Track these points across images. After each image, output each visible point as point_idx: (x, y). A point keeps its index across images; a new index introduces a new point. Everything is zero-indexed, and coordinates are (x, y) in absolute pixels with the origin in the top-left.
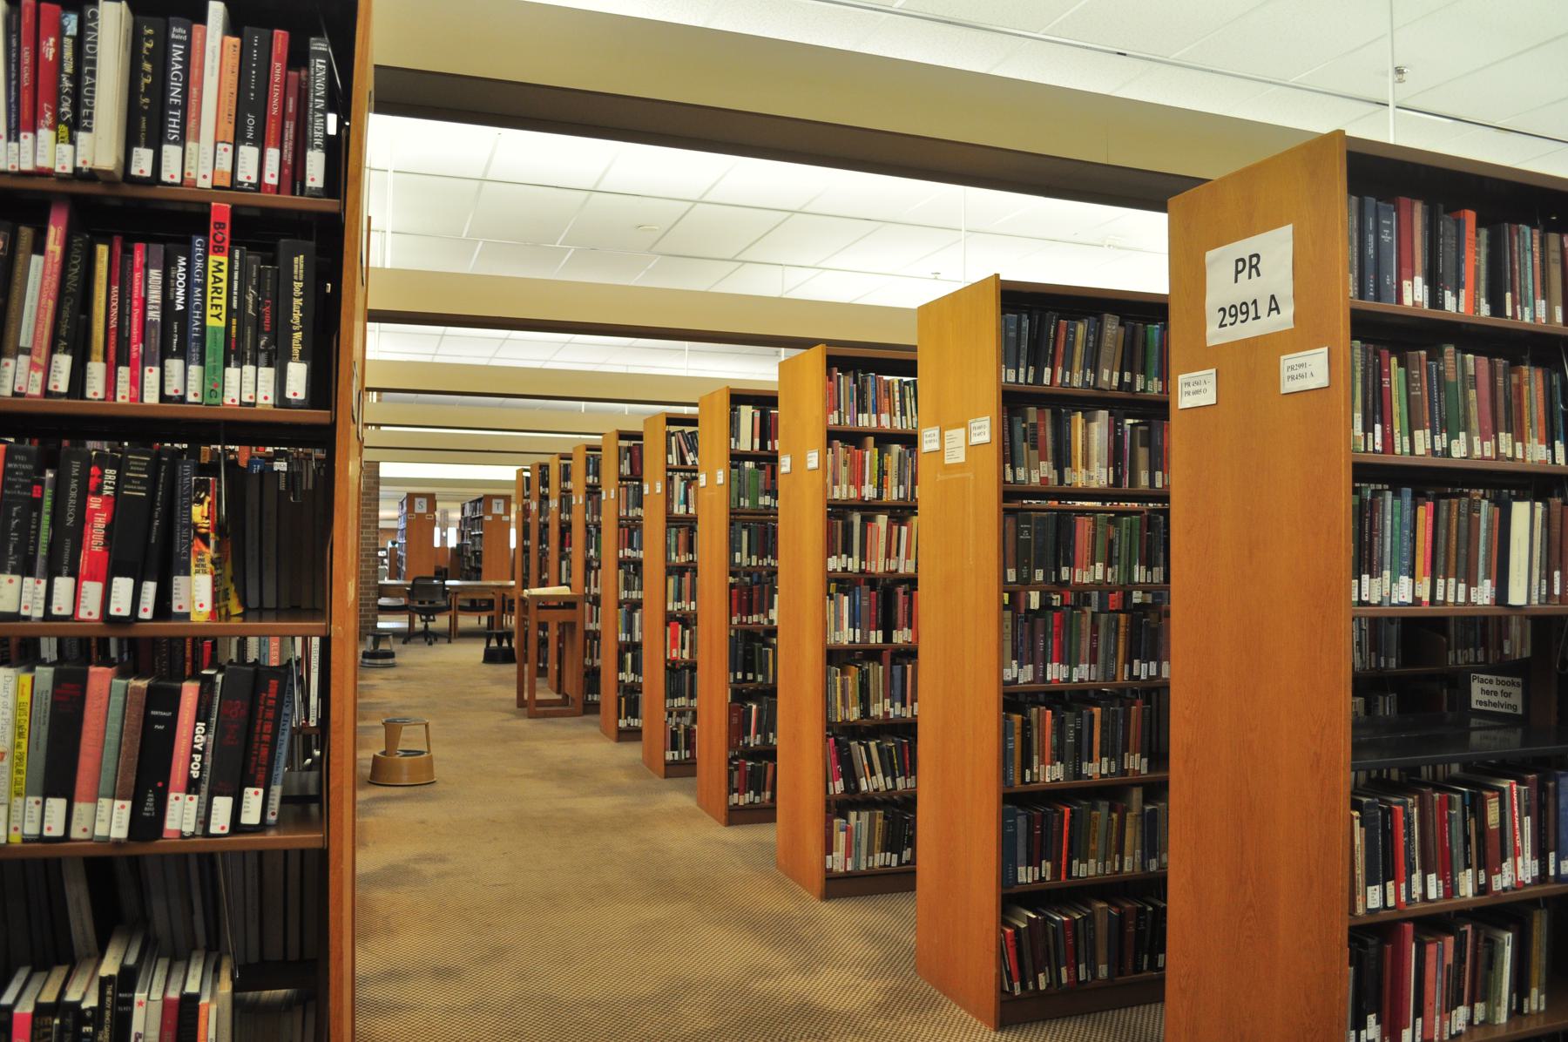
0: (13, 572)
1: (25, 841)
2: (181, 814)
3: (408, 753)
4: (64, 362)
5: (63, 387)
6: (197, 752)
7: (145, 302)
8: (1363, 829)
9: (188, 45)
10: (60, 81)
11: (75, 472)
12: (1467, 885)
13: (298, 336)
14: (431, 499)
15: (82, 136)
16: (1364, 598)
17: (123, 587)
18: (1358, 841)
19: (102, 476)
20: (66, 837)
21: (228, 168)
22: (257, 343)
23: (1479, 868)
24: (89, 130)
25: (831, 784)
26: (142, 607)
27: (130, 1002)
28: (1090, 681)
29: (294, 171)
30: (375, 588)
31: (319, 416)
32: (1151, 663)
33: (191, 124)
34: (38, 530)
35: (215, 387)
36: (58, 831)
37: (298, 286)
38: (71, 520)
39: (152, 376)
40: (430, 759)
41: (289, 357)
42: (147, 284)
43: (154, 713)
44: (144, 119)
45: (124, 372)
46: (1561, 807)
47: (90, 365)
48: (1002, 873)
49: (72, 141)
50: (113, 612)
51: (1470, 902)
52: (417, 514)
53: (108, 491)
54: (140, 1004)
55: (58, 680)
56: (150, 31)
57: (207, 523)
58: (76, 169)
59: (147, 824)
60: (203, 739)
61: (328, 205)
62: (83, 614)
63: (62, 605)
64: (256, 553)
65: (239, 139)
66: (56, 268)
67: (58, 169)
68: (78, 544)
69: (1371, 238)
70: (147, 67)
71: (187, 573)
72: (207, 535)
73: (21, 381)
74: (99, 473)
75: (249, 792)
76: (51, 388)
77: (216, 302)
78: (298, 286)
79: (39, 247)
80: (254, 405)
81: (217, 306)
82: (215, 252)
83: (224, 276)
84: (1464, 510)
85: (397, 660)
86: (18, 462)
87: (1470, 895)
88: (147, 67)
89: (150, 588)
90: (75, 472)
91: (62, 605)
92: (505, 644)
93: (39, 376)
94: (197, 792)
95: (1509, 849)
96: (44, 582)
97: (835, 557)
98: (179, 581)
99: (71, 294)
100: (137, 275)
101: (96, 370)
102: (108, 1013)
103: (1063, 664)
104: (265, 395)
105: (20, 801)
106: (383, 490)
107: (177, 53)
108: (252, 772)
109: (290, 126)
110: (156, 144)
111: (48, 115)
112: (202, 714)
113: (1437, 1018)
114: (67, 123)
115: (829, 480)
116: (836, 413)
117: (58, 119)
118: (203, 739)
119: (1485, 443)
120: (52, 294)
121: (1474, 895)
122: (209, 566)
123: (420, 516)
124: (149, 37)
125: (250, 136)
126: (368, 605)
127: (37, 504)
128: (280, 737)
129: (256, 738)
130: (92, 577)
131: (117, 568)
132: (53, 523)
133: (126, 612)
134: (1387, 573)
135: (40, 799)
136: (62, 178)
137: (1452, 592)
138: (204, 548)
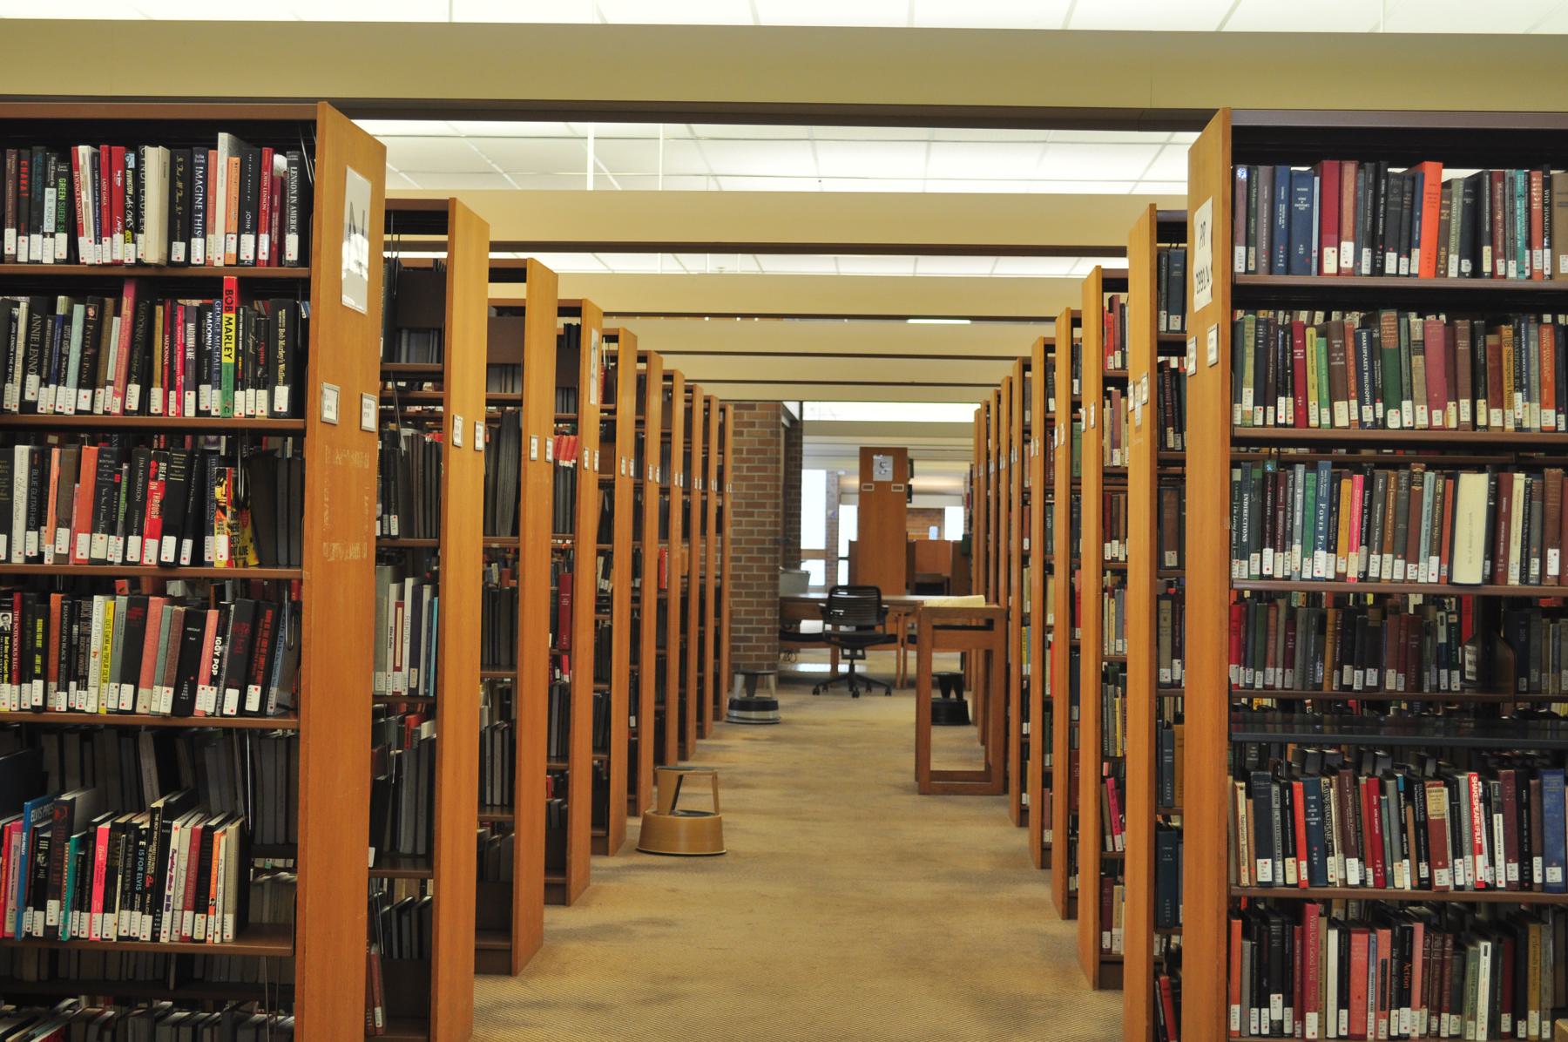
0: (103, 533)
1: (108, 712)
2: (206, 699)
3: (689, 813)
4: (135, 389)
5: (135, 407)
6: (216, 657)
7: (184, 346)
8: (1251, 801)
9: (206, 166)
10: (126, 201)
11: (141, 464)
12: (1403, 876)
13: (282, 367)
14: (903, 462)
15: (140, 237)
16: (1265, 572)
17: (170, 542)
18: (1242, 811)
19: (158, 467)
20: (133, 711)
21: (234, 251)
22: (256, 373)
23: (1419, 860)
24: (142, 232)
25: (1109, 838)
26: (182, 556)
27: (169, 827)
28: (1283, 688)
29: (279, 249)
30: (773, 604)
31: (295, 423)
32: (1369, 671)
33: (210, 222)
34: (118, 504)
35: (229, 405)
36: (128, 707)
37: (282, 331)
38: (139, 497)
39: (190, 398)
40: (718, 825)
41: (276, 383)
42: (186, 334)
43: (189, 629)
44: (179, 222)
45: (173, 394)
46: (1546, 807)
47: (152, 389)
48: (569, 714)
49: (135, 241)
50: (163, 559)
51: (1407, 893)
52: (876, 483)
53: (161, 477)
54: (176, 829)
55: (130, 604)
56: (180, 160)
57: (224, 499)
58: (138, 260)
59: (183, 705)
60: (220, 648)
61: (301, 272)
62: (146, 561)
63: (133, 555)
64: (285, 522)
65: (241, 230)
66: (128, 326)
67: (126, 261)
68: (143, 514)
69: (1282, 208)
70: (180, 185)
71: (213, 535)
72: (225, 507)
73: (108, 403)
74: (156, 465)
75: (251, 688)
76: (127, 408)
77: (228, 346)
78: (282, 331)
79: (118, 312)
80: (254, 416)
81: (228, 349)
82: (227, 311)
83: (233, 327)
84: (1403, 482)
85: (782, 714)
86: (106, 459)
87: (1408, 887)
88: (180, 185)
89: (188, 544)
90: (141, 464)
91: (133, 555)
92: (953, 695)
93: (119, 400)
94: (217, 685)
95: (1467, 846)
96: (122, 539)
97: (1115, 542)
98: (208, 539)
99: (139, 343)
100: (179, 328)
101: (157, 393)
102: (156, 833)
103: (1245, 666)
104: (262, 410)
105: (106, 685)
106: (809, 443)
107: (199, 172)
108: (253, 674)
109: (276, 216)
110: (187, 238)
111: (119, 223)
112: (221, 631)
113: (1371, 1015)
114: (130, 229)
115: (1107, 441)
116: (1118, 354)
117: (125, 227)
118: (220, 648)
119: (1434, 412)
120: (126, 345)
121: (1412, 888)
122: (226, 529)
123: (882, 485)
124: (180, 163)
125: (248, 226)
126: (762, 630)
127: (117, 487)
128: (277, 653)
129: (257, 650)
130: (151, 537)
131: (167, 530)
132: (128, 499)
133: (171, 559)
134: (1297, 548)
135: (118, 685)
136: (130, 266)
137: (1389, 568)
138: (223, 517)
